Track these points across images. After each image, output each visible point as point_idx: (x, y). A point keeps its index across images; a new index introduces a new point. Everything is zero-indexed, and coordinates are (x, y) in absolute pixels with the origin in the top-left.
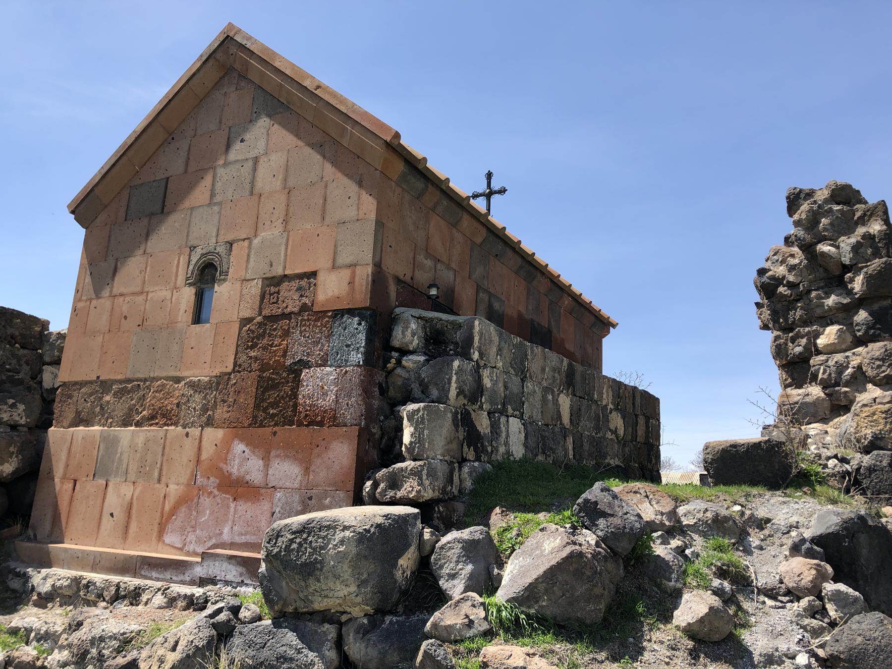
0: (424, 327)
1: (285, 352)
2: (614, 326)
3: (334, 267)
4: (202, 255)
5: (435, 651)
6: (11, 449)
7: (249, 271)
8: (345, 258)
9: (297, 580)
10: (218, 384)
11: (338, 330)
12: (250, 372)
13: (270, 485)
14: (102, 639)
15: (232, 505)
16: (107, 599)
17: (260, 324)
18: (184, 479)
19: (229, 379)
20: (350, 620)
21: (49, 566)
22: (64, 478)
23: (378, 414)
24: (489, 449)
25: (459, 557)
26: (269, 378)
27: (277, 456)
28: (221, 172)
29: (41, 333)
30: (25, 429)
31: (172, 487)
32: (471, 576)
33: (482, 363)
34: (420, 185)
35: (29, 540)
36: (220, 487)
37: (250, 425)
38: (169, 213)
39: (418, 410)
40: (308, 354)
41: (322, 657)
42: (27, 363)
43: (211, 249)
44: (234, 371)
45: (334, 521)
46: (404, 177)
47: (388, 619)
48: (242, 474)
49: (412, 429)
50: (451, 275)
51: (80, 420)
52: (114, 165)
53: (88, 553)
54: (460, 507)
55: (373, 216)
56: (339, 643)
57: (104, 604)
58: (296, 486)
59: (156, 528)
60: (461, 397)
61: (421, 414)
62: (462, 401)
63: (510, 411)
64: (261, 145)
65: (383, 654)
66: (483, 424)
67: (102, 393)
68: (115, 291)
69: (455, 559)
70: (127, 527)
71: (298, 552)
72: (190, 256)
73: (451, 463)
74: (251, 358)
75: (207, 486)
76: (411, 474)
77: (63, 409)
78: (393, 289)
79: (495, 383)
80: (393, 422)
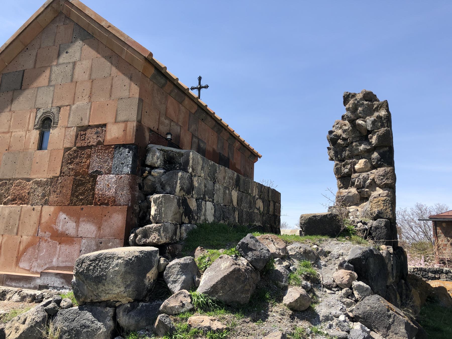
0: (164, 155)
1: (88, 166)
2: (260, 157)
3: (116, 122)
4: (44, 113)
5: (165, 320)
7: (70, 123)
8: (121, 117)
9: (93, 285)
10: (51, 182)
11: (117, 155)
12: (69, 176)
13: (79, 236)
15: (58, 247)
17: (75, 151)
18: (31, 232)
19: (57, 180)
23: (138, 200)
24: (196, 218)
25: (178, 272)
26: (80, 180)
27: (84, 221)
28: (54, 68)
31: (25, 238)
33: (193, 174)
34: (163, 81)
36: (52, 237)
37: (69, 205)
38: (25, 89)
39: (159, 198)
40: (101, 167)
41: (105, 325)
43: (49, 110)
44: (60, 176)
45: (113, 255)
48: (64, 230)
49: (156, 207)
50: (179, 128)
54: (180, 247)
55: (137, 96)
56: (115, 317)
60: (182, 191)
62: (183, 193)
63: (207, 198)
64: (77, 56)
65: (138, 322)
66: (193, 205)
69: (176, 273)
71: (93, 271)
72: (36, 113)
73: (176, 225)
74: (70, 169)
75: (44, 236)
78: (147, 134)
79: (200, 184)
80: (146, 204)
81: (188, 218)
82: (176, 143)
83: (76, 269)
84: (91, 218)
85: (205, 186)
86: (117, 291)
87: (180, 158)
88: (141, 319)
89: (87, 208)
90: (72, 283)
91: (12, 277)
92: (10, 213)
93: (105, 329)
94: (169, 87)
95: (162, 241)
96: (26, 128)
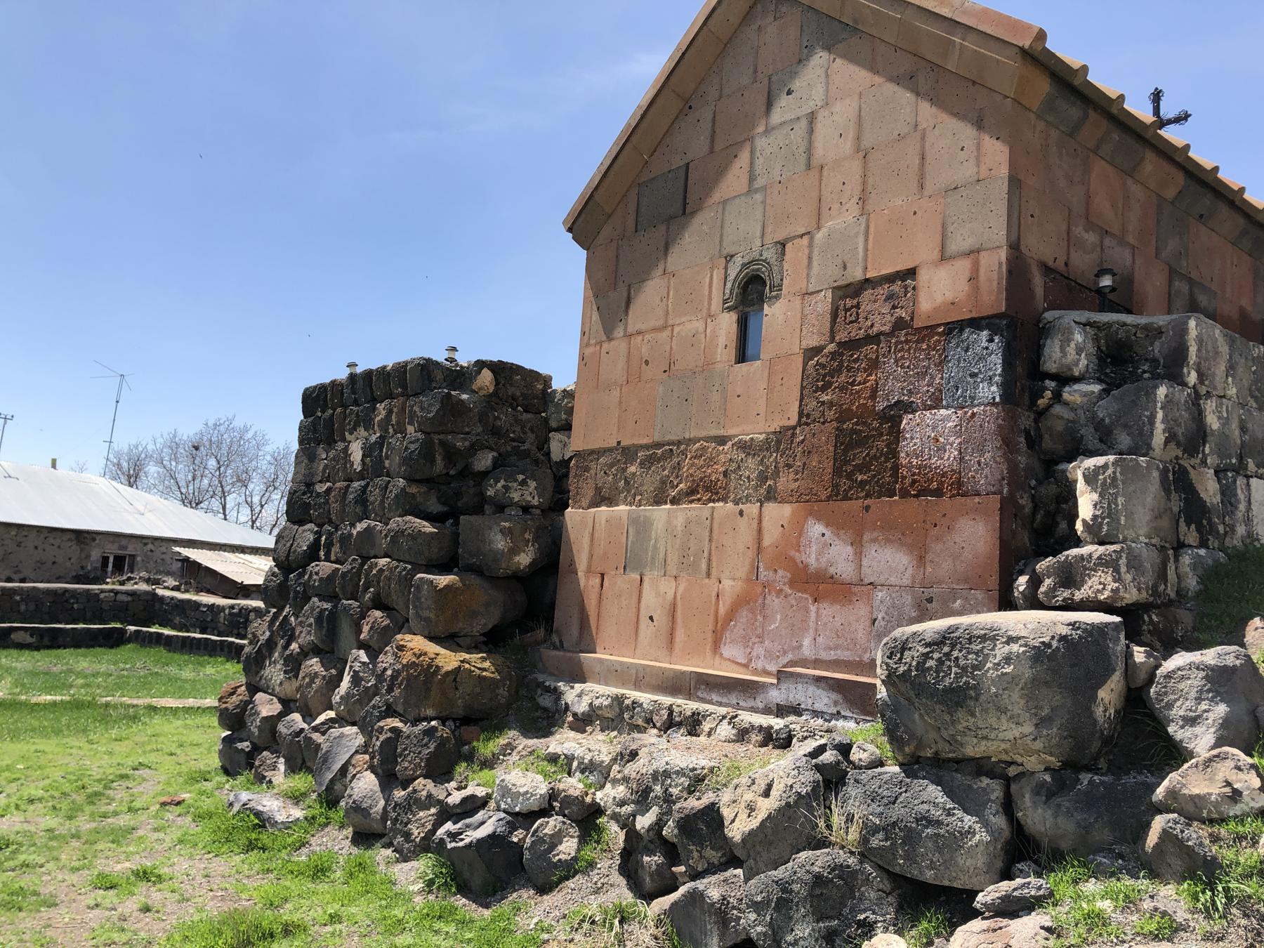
0: (1096, 339)
1: (874, 391)
3: (944, 257)
4: (744, 265)
5: (1182, 832)
6: (527, 536)
7: (813, 280)
8: (961, 240)
9: (938, 711)
10: (779, 442)
11: (955, 353)
12: (823, 423)
13: (867, 581)
14: (667, 774)
15: (813, 608)
16: (658, 725)
17: (833, 355)
18: (742, 570)
19: (794, 435)
20: (1022, 775)
21: (583, 680)
22: (589, 571)
23: (1026, 478)
24: (1221, 528)
25: (1201, 692)
26: (853, 431)
27: (874, 540)
28: (761, 143)
29: (544, 391)
30: (538, 511)
31: (727, 583)
32: (1226, 723)
33: (1203, 390)
34: (1074, 112)
35: (555, 648)
36: (792, 583)
37: (829, 498)
38: (693, 213)
39: (1105, 466)
40: (910, 392)
41: (986, 824)
42: (532, 430)
43: (756, 255)
44: (799, 423)
45: (992, 629)
46: (1058, 107)
47: (1085, 778)
48: (823, 565)
49: (1095, 497)
50: (1127, 254)
51: (603, 498)
52: (616, 157)
53: (629, 666)
54: (1186, 618)
55: (1004, 171)
56: (1008, 807)
57: (655, 731)
58: (906, 581)
59: (709, 636)
60: (1172, 445)
61: (1110, 471)
62: (1174, 451)
63: (1251, 466)
64: (818, 94)
65: (1086, 828)
66: (1209, 488)
67: (625, 463)
68: (630, 329)
69: (1193, 694)
70: (672, 634)
71: (937, 672)
72: (726, 268)
73: (1162, 549)
74: (823, 403)
75: (774, 581)
76: (1101, 565)
77: (580, 486)
78: (1038, 282)
79: (1226, 422)
80: (1051, 489)
81: (1198, 531)
82: (1122, 298)
83: (887, 664)
84: (895, 533)
85: (1243, 429)
86: (1012, 733)
87: (1152, 344)
88: (1096, 821)
89: (881, 505)
90: (880, 702)
91: (711, 679)
92: (688, 522)
93: (986, 837)
94: (1095, 128)
95: (1127, 596)
96: (705, 311)
